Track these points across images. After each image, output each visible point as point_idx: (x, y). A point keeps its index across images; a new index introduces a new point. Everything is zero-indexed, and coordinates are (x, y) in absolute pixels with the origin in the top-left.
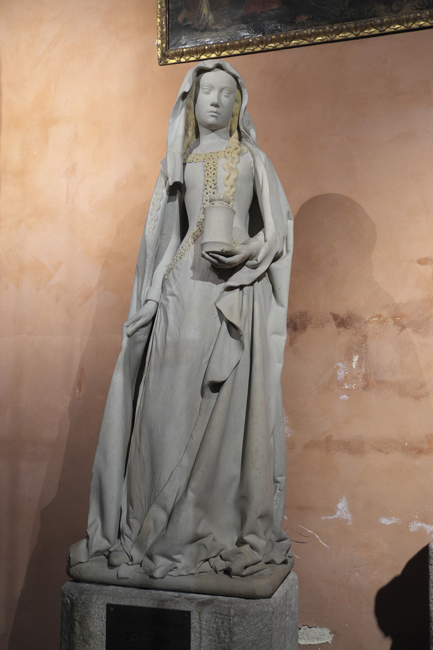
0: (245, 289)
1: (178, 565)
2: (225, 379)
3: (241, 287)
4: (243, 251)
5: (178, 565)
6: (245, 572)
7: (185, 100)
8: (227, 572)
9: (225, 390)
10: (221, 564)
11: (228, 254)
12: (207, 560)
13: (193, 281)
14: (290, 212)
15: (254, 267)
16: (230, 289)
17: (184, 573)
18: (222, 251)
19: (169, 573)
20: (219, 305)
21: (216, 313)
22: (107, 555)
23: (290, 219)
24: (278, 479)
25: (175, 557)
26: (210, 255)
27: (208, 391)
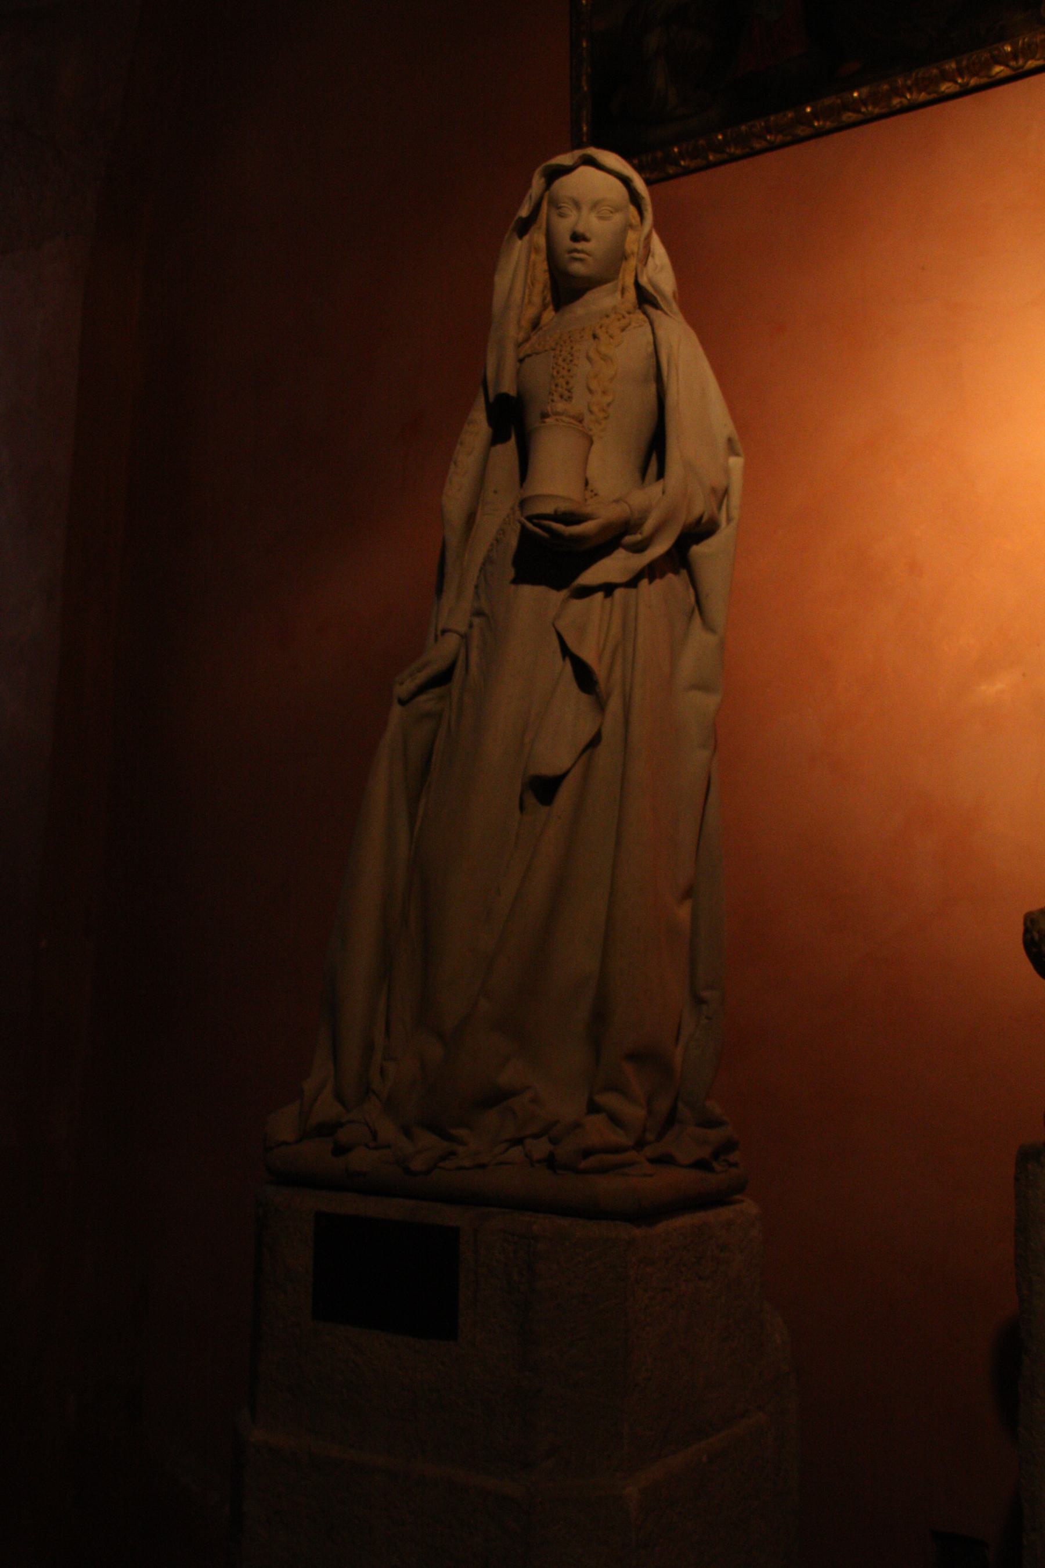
0: (618, 593)
1: (460, 1149)
2: (564, 770)
3: (608, 589)
4: (604, 512)
5: (460, 1149)
6: (583, 1165)
7: (526, 238)
8: (550, 1162)
9: (565, 794)
10: (541, 1148)
11: (572, 518)
12: (519, 1141)
13: (513, 587)
14: (736, 437)
15: (639, 548)
16: (585, 592)
17: (467, 1163)
18: (556, 511)
19: (442, 1164)
20: (561, 625)
21: (556, 643)
22: (327, 1129)
23: (737, 454)
24: (706, 994)
25: (454, 1132)
26: (535, 525)
27: (531, 800)
